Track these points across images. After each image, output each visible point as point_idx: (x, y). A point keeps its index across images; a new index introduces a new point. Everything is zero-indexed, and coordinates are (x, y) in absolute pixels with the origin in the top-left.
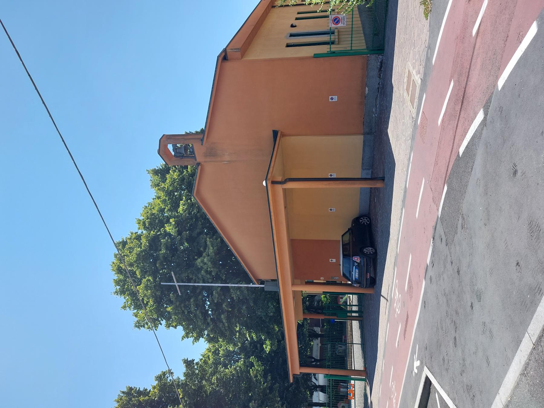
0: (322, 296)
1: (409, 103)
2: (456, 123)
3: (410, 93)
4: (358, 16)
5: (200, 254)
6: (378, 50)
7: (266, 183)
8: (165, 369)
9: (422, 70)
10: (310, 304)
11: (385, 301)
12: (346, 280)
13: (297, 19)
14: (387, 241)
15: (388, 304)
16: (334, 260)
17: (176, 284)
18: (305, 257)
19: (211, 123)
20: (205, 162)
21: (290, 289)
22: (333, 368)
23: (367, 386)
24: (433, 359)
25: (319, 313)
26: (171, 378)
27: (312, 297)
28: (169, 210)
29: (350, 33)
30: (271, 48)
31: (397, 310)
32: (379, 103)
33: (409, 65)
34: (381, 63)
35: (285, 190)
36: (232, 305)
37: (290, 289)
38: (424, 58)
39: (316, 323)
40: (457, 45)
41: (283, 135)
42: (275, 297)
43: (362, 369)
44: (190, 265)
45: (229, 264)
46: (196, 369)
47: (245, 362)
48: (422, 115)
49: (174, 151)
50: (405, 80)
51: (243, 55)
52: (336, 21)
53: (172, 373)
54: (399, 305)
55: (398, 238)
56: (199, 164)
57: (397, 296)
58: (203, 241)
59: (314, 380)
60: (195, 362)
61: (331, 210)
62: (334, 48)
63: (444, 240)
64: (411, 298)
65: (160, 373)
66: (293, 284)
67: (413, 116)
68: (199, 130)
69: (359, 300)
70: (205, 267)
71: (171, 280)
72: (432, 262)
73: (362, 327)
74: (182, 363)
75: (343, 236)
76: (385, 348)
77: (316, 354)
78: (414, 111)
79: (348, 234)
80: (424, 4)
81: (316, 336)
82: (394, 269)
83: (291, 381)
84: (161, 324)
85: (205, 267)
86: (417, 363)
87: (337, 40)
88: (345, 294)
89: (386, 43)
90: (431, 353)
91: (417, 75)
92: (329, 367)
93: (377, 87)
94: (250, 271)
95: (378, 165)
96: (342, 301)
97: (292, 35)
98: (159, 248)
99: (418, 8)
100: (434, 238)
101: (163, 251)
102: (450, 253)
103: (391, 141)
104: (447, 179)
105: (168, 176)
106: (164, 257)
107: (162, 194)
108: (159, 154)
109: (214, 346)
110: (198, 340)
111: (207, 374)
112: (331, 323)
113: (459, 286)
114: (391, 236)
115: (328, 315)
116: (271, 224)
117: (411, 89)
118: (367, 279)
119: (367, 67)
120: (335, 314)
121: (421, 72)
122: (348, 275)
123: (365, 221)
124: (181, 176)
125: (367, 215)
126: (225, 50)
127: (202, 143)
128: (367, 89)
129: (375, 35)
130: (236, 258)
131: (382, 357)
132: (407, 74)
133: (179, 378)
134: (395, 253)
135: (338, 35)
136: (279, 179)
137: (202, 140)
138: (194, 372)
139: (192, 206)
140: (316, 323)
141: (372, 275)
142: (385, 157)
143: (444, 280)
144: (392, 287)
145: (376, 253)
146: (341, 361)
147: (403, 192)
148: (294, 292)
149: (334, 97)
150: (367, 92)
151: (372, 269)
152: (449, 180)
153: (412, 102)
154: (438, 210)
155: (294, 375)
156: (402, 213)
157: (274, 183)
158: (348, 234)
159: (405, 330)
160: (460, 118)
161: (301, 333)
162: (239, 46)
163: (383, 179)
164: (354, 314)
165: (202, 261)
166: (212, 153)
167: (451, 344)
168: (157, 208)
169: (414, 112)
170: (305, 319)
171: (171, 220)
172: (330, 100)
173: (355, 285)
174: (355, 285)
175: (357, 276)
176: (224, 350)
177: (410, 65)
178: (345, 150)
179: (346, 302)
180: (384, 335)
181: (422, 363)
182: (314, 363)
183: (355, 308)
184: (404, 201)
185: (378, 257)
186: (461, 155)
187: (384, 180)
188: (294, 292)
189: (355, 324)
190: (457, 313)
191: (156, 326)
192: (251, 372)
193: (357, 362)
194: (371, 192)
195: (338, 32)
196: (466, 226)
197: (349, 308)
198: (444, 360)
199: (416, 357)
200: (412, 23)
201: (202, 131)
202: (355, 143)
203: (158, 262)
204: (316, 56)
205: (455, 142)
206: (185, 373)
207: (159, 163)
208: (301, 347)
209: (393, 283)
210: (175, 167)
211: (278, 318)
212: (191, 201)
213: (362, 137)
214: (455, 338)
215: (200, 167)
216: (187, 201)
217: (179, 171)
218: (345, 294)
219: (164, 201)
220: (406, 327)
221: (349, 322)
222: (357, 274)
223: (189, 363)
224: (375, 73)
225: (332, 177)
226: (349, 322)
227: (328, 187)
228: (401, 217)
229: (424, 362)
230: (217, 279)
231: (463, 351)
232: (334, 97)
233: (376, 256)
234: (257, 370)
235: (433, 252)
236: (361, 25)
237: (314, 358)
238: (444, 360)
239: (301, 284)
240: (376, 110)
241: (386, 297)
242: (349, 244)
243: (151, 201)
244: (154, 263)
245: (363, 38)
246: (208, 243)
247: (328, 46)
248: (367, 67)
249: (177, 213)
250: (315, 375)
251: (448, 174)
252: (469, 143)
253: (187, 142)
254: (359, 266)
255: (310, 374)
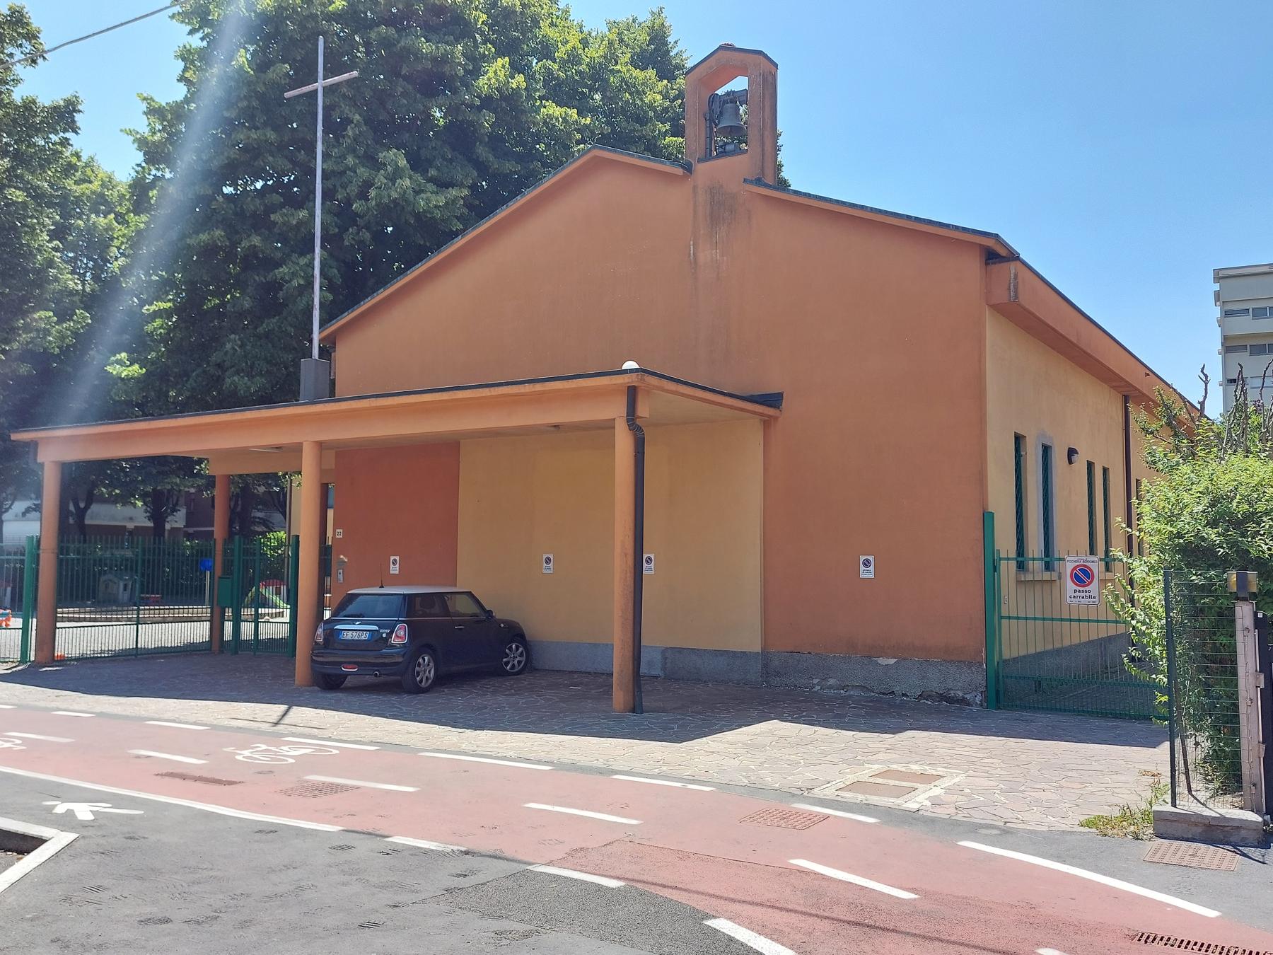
0: (282, 534)
1: (851, 778)
2: (799, 908)
3: (880, 781)
4: (1094, 637)
5: (417, 163)
6: (997, 692)
7: (631, 371)
8: (46, 41)
9: (942, 812)
10: (259, 498)
11: (274, 718)
12: (335, 605)
13: (1090, 466)
14: (454, 724)
15: (265, 727)
16: (394, 570)
17: (320, 85)
18: (407, 482)
19: (807, 208)
20: (695, 187)
21: (308, 437)
22: (61, 564)
23: (6, 666)
24: (98, 858)
25: (231, 523)
26: (18, 55)
27: (280, 503)
28: (549, 71)
29: (1048, 616)
30: (1017, 394)
31: (247, 753)
32: (851, 696)
33: (959, 778)
34: (963, 701)
35: (609, 425)
36: (253, 261)
37: (308, 437)
38: (978, 817)
39: (201, 514)
40: (1012, 906)
41: (767, 423)
42: (282, 390)
43: (59, 652)
44: (385, 130)
45: (380, 255)
46: (47, 140)
47: (72, 293)
48: (818, 814)
49: (728, 94)
50: (914, 767)
51: (998, 309)
52: (1081, 575)
53: (34, 62)
54: (262, 759)
55: (465, 754)
56: (688, 168)
57: (291, 752)
58: (459, 177)
59: (19, 506)
60: (69, 135)
61: (548, 561)
62: (1008, 570)
63: (462, 882)
64: (287, 792)
65: (35, 22)
66: (321, 446)
67: (816, 791)
68: (785, 174)
69: (273, 643)
70: (381, 179)
71: (329, 73)
72: (395, 851)
73: (188, 651)
74: (67, 95)
75: (470, 594)
76: (127, 717)
77: (100, 515)
78: (830, 792)
79: (474, 609)
80: (1124, 817)
81: (158, 517)
82: (371, 743)
83: (14, 437)
84: (191, 32)
85: (381, 179)
86: (83, 812)
87: (1029, 577)
88: (292, 599)
89: (1017, 714)
90: (117, 850)
91: (929, 798)
92: (62, 549)
93: (897, 689)
94: (363, 315)
95: (678, 693)
96: (268, 592)
97: (1046, 450)
98: (434, 37)
99: (1113, 800)
100: (467, 853)
101: (426, 48)
102: (423, 901)
103: (744, 729)
104: (639, 885)
105: (651, 73)
106: (408, 51)
107: (595, 52)
108: (721, 48)
109: (122, 197)
110: (140, 149)
111: (33, 173)
112: (201, 558)
113: (326, 929)
114: (469, 733)
115: (225, 551)
116: (508, 384)
117: (892, 782)
118: (340, 663)
119: (951, 662)
120: (228, 566)
121: (938, 809)
122: (351, 609)
123: (514, 657)
124: (651, 114)
125: (529, 667)
126: (1013, 257)
127: (751, 182)
128: (892, 661)
129: (1039, 684)
130: (401, 272)
131: (98, 709)
132: (930, 770)
133: (17, 81)
134: (419, 745)
135: (1042, 582)
136: (643, 410)
137: (759, 182)
138: (38, 130)
139: (561, 143)
140: (201, 514)
141: (349, 681)
142: (700, 713)
143: (343, 884)
144: (315, 737)
145: (417, 690)
146: (83, 588)
147: (600, 764)
148: (297, 449)
149: (871, 568)
150: (883, 661)
151: (369, 679)
152: (635, 892)
153: (852, 787)
154: (550, 863)
155: (33, 446)
156: (539, 762)
157: (632, 393)
158: (474, 609)
159: (184, 777)
160: (811, 920)
161: (167, 468)
162: (1025, 300)
163: (636, 708)
164: (228, 626)
165: (397, 174)
166: (720, 209)
167: (148, 910)
168: (553, 34)
169: (827, 792)
170: (211, 482)
171: (520, 78)
172: (862, 558)
173: (320, 631)
174: (320, 631)
175: (349, 636)
176: (109, 228)
177: (956, 780)
178: (719, 598)
179: (265, 604)
180: (166, 716)
181: (85, 825)
182: (72, 508)
183: (247, 630)
184: (574, 768)
185: (406, 697)
186: (710, 923)
187: (633, 710)
188: (297, 449)
189: (199, 632)
190: (245, 924)
191: (184, 17)
192: (42, 314)
193: (81, 636)
194: (597, 674)
195: (1051, 582)
196: (504, 942)
197: (248, 612)
198: (98, 889)
199: (104, 807)
200: (1069, 785)
201: (783, 185)
202: (736, 624)
203: (392, 31)
204: (987, 519)
205: (735, 904)
206: (34, 102)
207: (691, 47)
208: (123, 469)
209: (329, 739)
210: (676, 98)
211: (215, 397)
212: (578, 143)
213: (757, 648)
214: (167, 921)
215: (680, 171)
216: (578, 131)
217: (666, 110)
218: (292, 599)
219: (573, 59)
220: (197, 779)
221: (205, 611)
222: (355, 636)
223: (65, 115)
224: (935, 685)
225: (645, 564)
226: (205, 611)
227: (618, 550)
228: (528, 760)
229: (90, 832)
230: (342, 215)
231: (128, 944)
232: (871, 568)
233: (410, 692)
234: (47, 332)
235: (427, 852)
236: (1067, 643)
237: (87, 507)
238: (98, 889)
239: (322, 472)
240: (831, 687)
241: (287, 720)
242: (447, 613)
243: (575, 16)
244: (391, 21)
245: (1032, 651)
246: (453, 192)
247: (1013, 554)
248: (951, 662)
249: (541, 98)
250: (38, 508)
251: (652, 889)
252: (742, 944)
253: (752, 134)
254: (378, 642)
255: (39, 495)
